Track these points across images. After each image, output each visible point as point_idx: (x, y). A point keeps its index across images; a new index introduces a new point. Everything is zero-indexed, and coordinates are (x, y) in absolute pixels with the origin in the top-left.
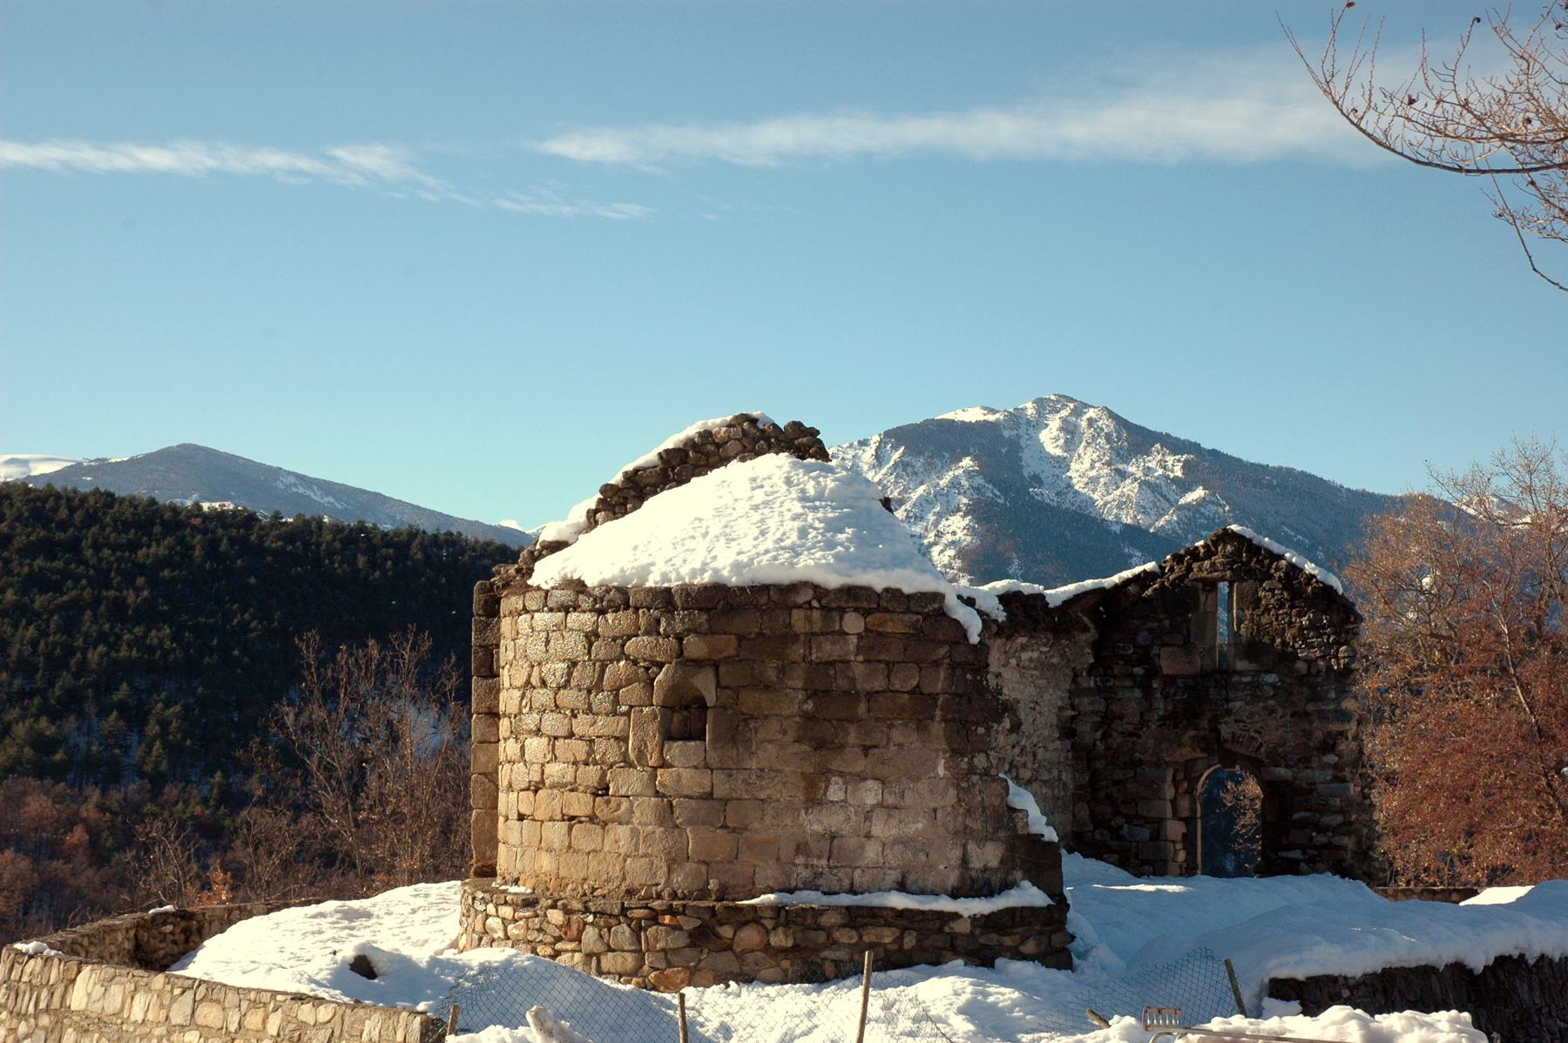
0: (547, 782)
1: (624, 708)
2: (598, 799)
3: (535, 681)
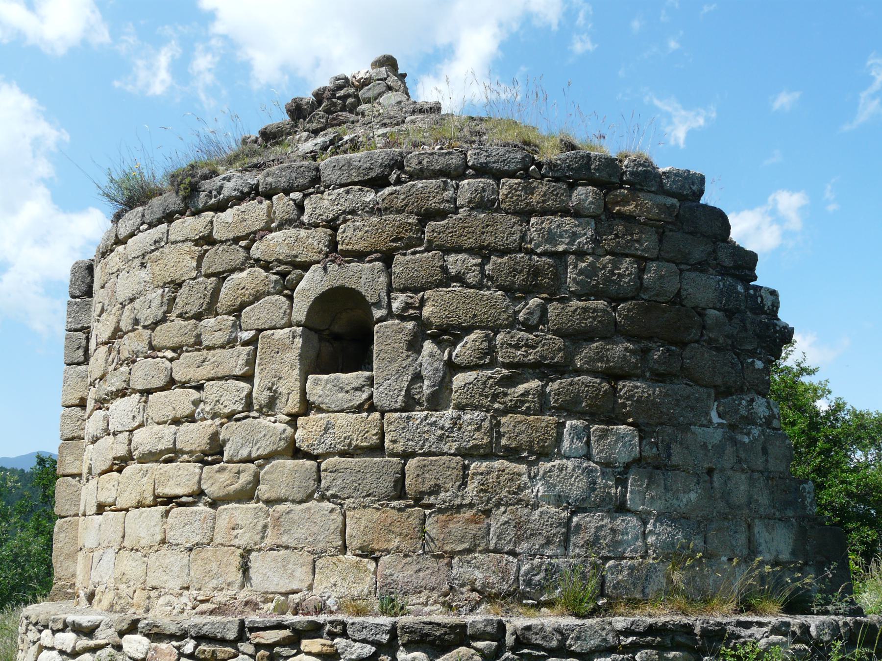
0: (136, 454)
1: (246, 335)
2: (206, 468)
3: (125, 325)
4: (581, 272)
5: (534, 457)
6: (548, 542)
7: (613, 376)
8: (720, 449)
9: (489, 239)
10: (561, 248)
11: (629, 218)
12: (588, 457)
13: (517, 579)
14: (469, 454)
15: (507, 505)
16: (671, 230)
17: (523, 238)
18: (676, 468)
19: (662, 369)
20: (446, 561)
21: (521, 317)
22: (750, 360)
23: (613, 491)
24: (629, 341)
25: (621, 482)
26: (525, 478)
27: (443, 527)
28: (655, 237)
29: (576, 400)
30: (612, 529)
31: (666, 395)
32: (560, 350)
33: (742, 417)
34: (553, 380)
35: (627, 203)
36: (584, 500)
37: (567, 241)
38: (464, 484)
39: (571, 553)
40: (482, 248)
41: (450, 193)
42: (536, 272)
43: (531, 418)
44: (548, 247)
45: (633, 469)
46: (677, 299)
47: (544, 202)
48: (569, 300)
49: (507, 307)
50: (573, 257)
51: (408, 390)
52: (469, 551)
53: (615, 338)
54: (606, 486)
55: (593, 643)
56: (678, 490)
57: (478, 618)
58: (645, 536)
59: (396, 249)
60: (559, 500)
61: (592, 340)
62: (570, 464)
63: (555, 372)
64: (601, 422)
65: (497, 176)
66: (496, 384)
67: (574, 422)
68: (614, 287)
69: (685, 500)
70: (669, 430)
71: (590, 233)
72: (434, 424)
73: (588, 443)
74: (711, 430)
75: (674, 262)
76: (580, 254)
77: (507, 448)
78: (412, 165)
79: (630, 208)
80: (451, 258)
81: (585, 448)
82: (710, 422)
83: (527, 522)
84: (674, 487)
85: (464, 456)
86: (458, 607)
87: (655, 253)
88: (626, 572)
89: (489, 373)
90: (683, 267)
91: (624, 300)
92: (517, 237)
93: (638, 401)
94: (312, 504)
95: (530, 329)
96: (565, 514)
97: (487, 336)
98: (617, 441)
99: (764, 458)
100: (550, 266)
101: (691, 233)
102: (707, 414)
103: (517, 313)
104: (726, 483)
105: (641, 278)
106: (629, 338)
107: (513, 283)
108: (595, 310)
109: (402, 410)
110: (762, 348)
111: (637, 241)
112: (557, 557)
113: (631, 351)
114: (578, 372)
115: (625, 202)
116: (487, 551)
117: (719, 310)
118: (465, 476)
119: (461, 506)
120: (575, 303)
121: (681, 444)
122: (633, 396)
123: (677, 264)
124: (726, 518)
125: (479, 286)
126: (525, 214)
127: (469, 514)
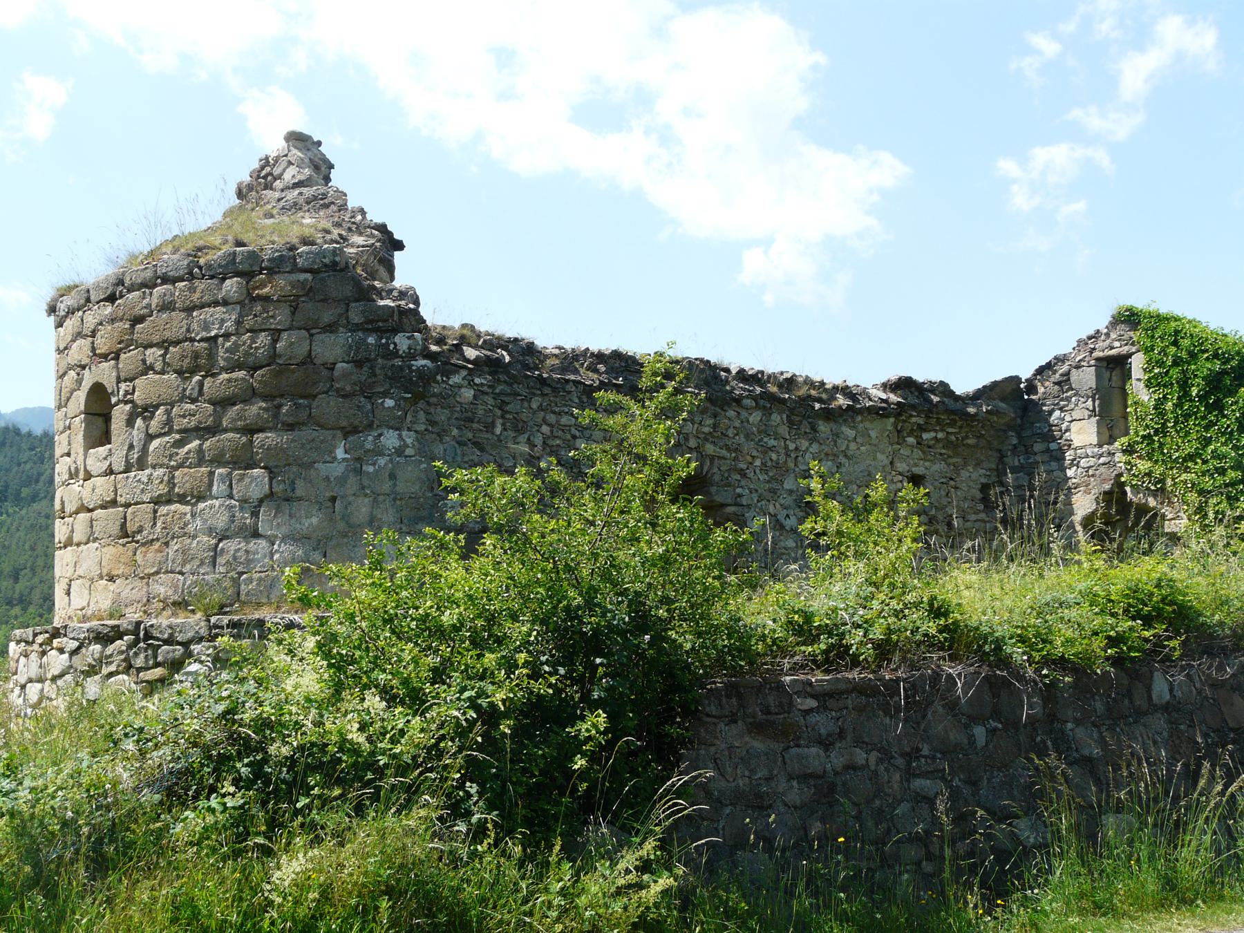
4: (227, 351)
5: (194, 500)
6: (202, 563)
7: (250, 431)
8: (342, 480)
9: (167, 334)
10: (213, 334)
11: (266, 299)
12: (231, 497)
13: (183, 591)
14: (157, 501)
15: (178, 537)
16: (303, 302)
17: (188, 330)
18: (300, 499)
19: (290, 420)
20: (146, 580)
21: (188, 393)
22: (380, 401)
23: (248, 521)
24: (263, 401)
25: (255, 514)
26: (188, 516)
27: (145, 556)
28: (287, 311)
29: (222, 454)
30: (246, 551)
31: (293, 441)
32: (210, 415)
33: (367, 451)
34: (207, 440)
35: (265, 286)
36: (227, 530)
37: (217, 326)
38: (155, 524)
39: (217, 571)
40: (164, 341)
41: (146, 301)
42: (196, 356)
43: (192, 470)
44: (204, 334)
45: (265, 504)
46: (309, 359)
47: (202, 297)
48: (219, 374)
49: (178, 386)
50: (221, 339)
51: (127, 457)
52: (157, 573)
53: (253, 400)
54: (243, 518)
55: (190, 634)
56: (301, 517)
57: (179, 621)
58: (272, 555)
59: (121, 349)
60: (210, 531)
61: (234, 404)
62: (217, 503)
63: (209, 432)
64: (240, 469)
65: (174, 281)
66: (171, 447)
67: (220, 470)
68: (251, 359)
69: (307, 525)
70: (295, 469)
71: (234, 317)
72: (139, 481)
73: (231, 486)
74: (335, 464)
75: (305, 329)
76: (227, 336)
77: (178, 495)
78: (127, 282)
79: (266, 290)
80: (149, 351)
81: (228, 490)
82: (335, 458)
83: (189, 549)
84: (298, 515)
85: (155, 504)
86: (151, 613)
87: (287, 324)
88: (255, 583)
89: (167, 439)
90: (313, 331)
91: (261, 367)
92: (184, 329)
93: (268, 449)
94: (91, 544)
95: (193, 401)
96: (214, 541)
97: (166, 410)
98: (251, 483)
99: (390, 483)
100: (206, 349)
101: (322, 301)
102: (332, 452)
103: (184, 390)
104: (346, 507)
105: (275, 348)
106: (265, 398)
107: (182, 366)
108: (236, 380)
109: (125, 472)
110: (396, 387)
111: (272, 317)
112: (208, 574)
113: (264, 409)
114: (226, 431)
115: (263, 285)
116: (167, 572)
117: (347, 362)
118: (155, 518)
119: (153, 540)
120: (224, 376)
121: (305, 479)
122: (264, 445)
123: (308, 330)
124: (346, 536)
125: (163, 372)
126: (189, 310)
127: (157, 545)
